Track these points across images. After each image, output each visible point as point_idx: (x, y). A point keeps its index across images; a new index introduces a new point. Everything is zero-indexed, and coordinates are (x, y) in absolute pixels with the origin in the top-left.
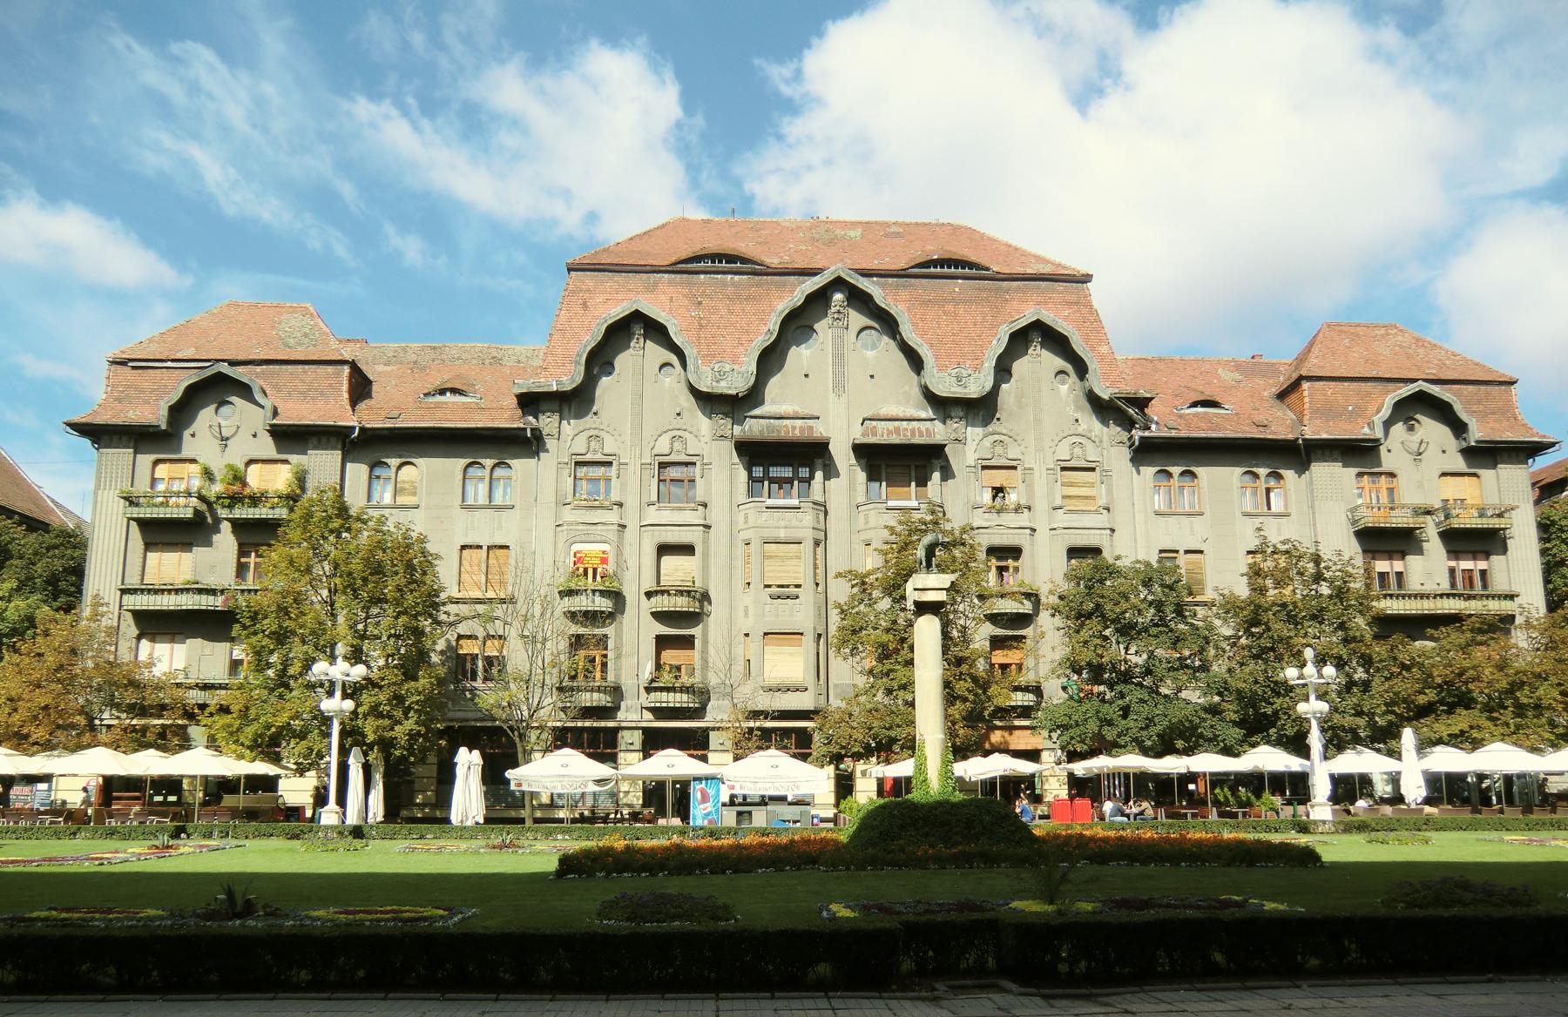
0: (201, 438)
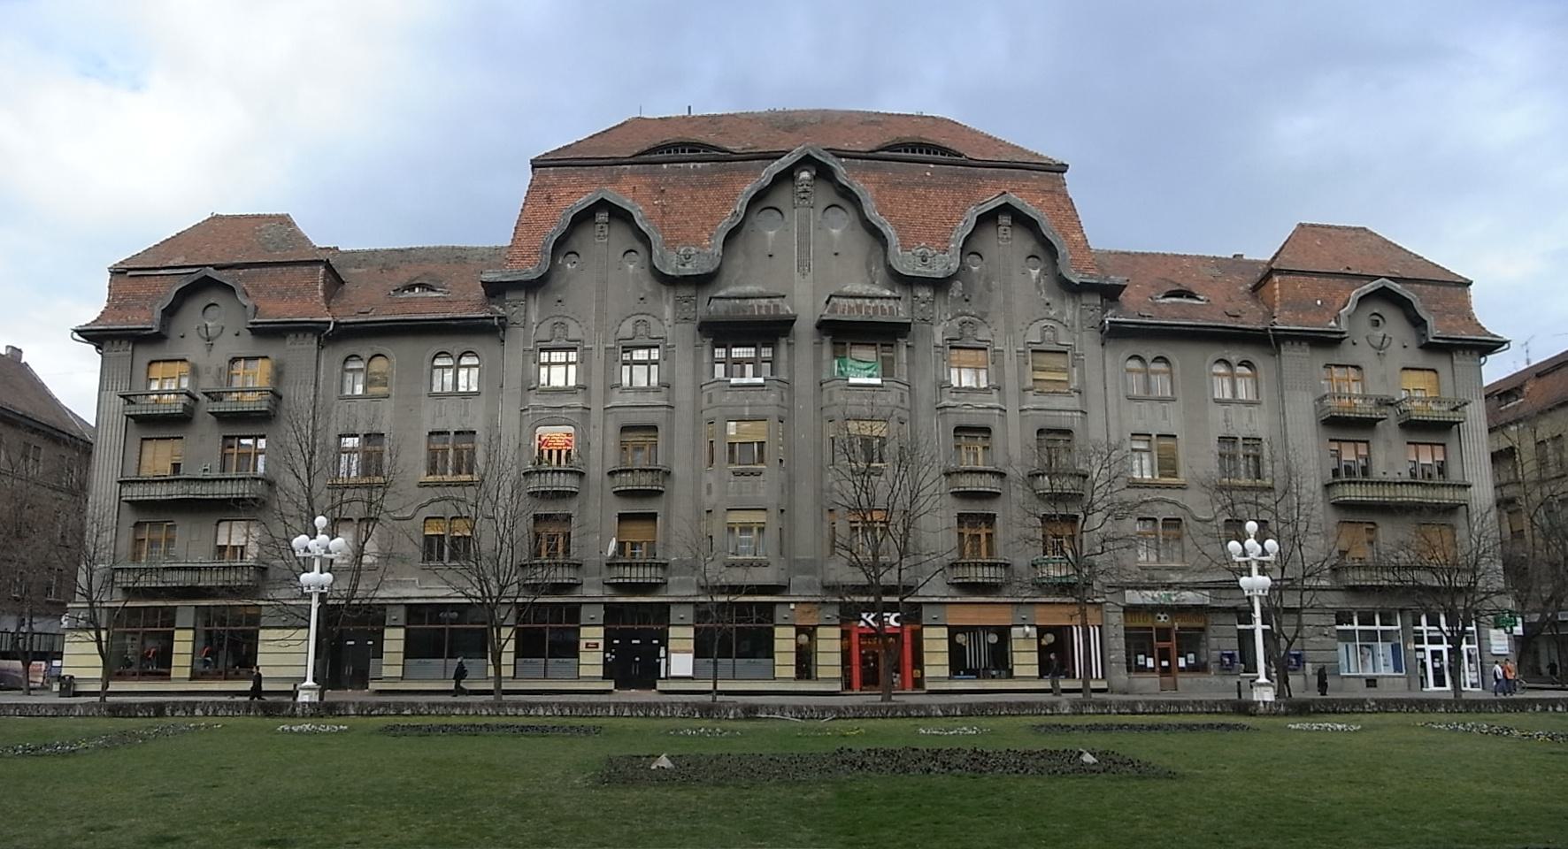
0: (189, 340)
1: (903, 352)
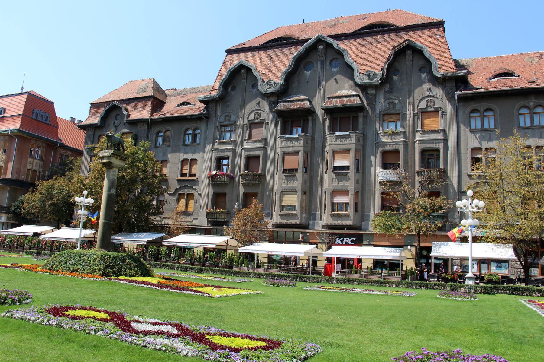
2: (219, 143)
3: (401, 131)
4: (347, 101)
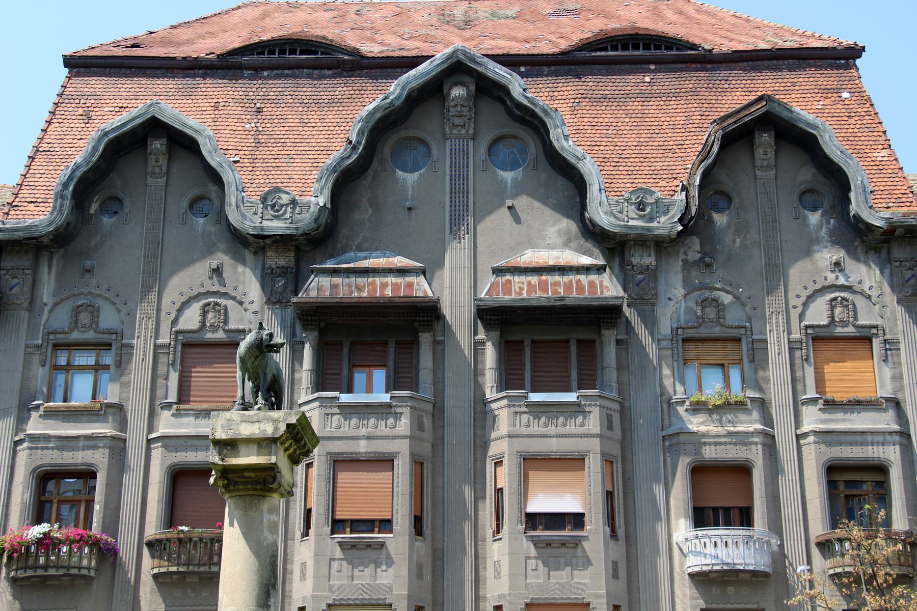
1: (682, 318)
2: (50, 414)
3: (753, 400)
4: (568, 287)
